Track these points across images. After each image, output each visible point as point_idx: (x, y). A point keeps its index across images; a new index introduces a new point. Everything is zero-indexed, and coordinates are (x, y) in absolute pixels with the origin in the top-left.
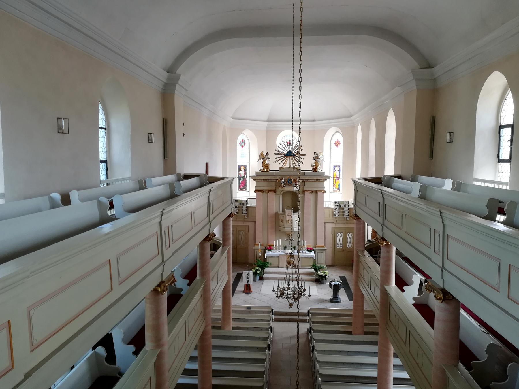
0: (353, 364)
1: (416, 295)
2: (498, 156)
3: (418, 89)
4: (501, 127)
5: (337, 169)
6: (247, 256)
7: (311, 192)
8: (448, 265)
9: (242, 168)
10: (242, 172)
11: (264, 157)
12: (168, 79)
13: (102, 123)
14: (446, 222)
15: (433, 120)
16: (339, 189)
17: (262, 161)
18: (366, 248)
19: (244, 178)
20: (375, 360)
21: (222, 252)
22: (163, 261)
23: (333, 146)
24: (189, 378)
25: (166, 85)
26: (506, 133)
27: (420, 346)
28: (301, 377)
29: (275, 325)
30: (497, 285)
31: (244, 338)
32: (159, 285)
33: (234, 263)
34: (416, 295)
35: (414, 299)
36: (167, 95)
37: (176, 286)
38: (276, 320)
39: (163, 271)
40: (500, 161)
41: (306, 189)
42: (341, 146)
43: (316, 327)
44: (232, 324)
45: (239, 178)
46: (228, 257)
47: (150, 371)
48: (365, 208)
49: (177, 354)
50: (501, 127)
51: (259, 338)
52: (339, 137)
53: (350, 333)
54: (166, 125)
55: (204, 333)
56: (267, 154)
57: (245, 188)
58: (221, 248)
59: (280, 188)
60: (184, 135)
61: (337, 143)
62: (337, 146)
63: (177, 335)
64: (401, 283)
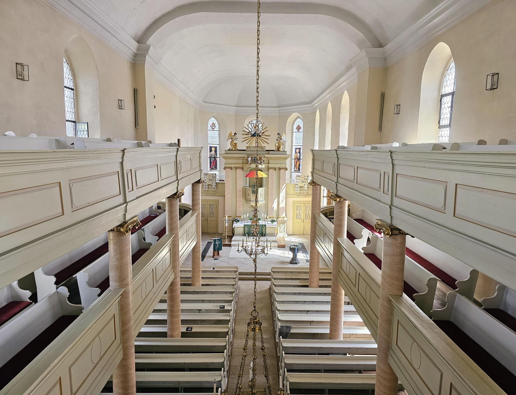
0: (309, 311)
1: (365, 246)
2: (439, 123)
3: (370, 67)
4: (442, 96)
5: (297, 151)
6: (217, 227)
7: (275, 169)
8: (397, 202)
9: (213, 149)
10: (213, 152)
11: (233, 137)
12: (138, 49)
13: (68, 82)
14: (395, 162)
15: (383, 95)
16: (299, 169)
17: (230, 140)
18: (321, 212)
19: (215, 158)
20: (328, 298)
21: (192, 215)
22: (126, 202)
23: (295, 130)
24: (160, 327)
25: (136, 55)
26: (447, 100)
27: (368, 284)
28: (268, 362)
29: (241, 283)
30: (443, 207)
31: (213, 293)
32: (121, 226)
33: (203, 233)
34: (365, 246)
35: (363, 249)
36: (137, 63)
37: (146, 241)
38: (240, 279)
39: (126, 211)
40: (440, 127)
41: (270, 166)
42: (301, 130)
43: (277, 282)
44: (202, 282)
45: (210, 158)
46: (197, 221)
47: (114, 309)
48: (321, 173)
49: (144, 298)
50: (442, 96)
51: (226, 293)
52: (299, 122)
53: (307, 286)
54: (137, 94)
55: (172, 284)
56: (235, 134)
57: (216, 168)
58: (191, 211)
59: (247, 165)
60: (155, 107)
61: (299, 128)
62: (298, 130)
63: (145, 280)
64: (351, 237)
